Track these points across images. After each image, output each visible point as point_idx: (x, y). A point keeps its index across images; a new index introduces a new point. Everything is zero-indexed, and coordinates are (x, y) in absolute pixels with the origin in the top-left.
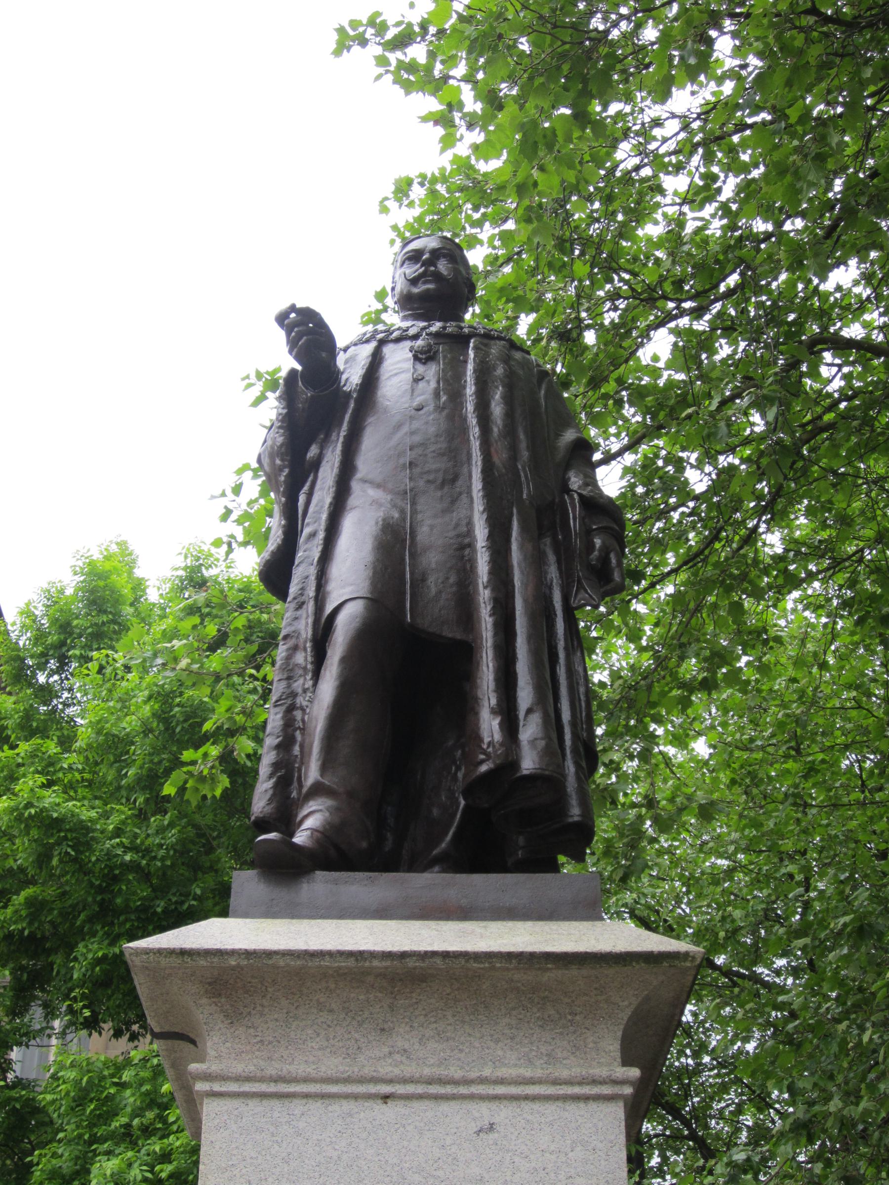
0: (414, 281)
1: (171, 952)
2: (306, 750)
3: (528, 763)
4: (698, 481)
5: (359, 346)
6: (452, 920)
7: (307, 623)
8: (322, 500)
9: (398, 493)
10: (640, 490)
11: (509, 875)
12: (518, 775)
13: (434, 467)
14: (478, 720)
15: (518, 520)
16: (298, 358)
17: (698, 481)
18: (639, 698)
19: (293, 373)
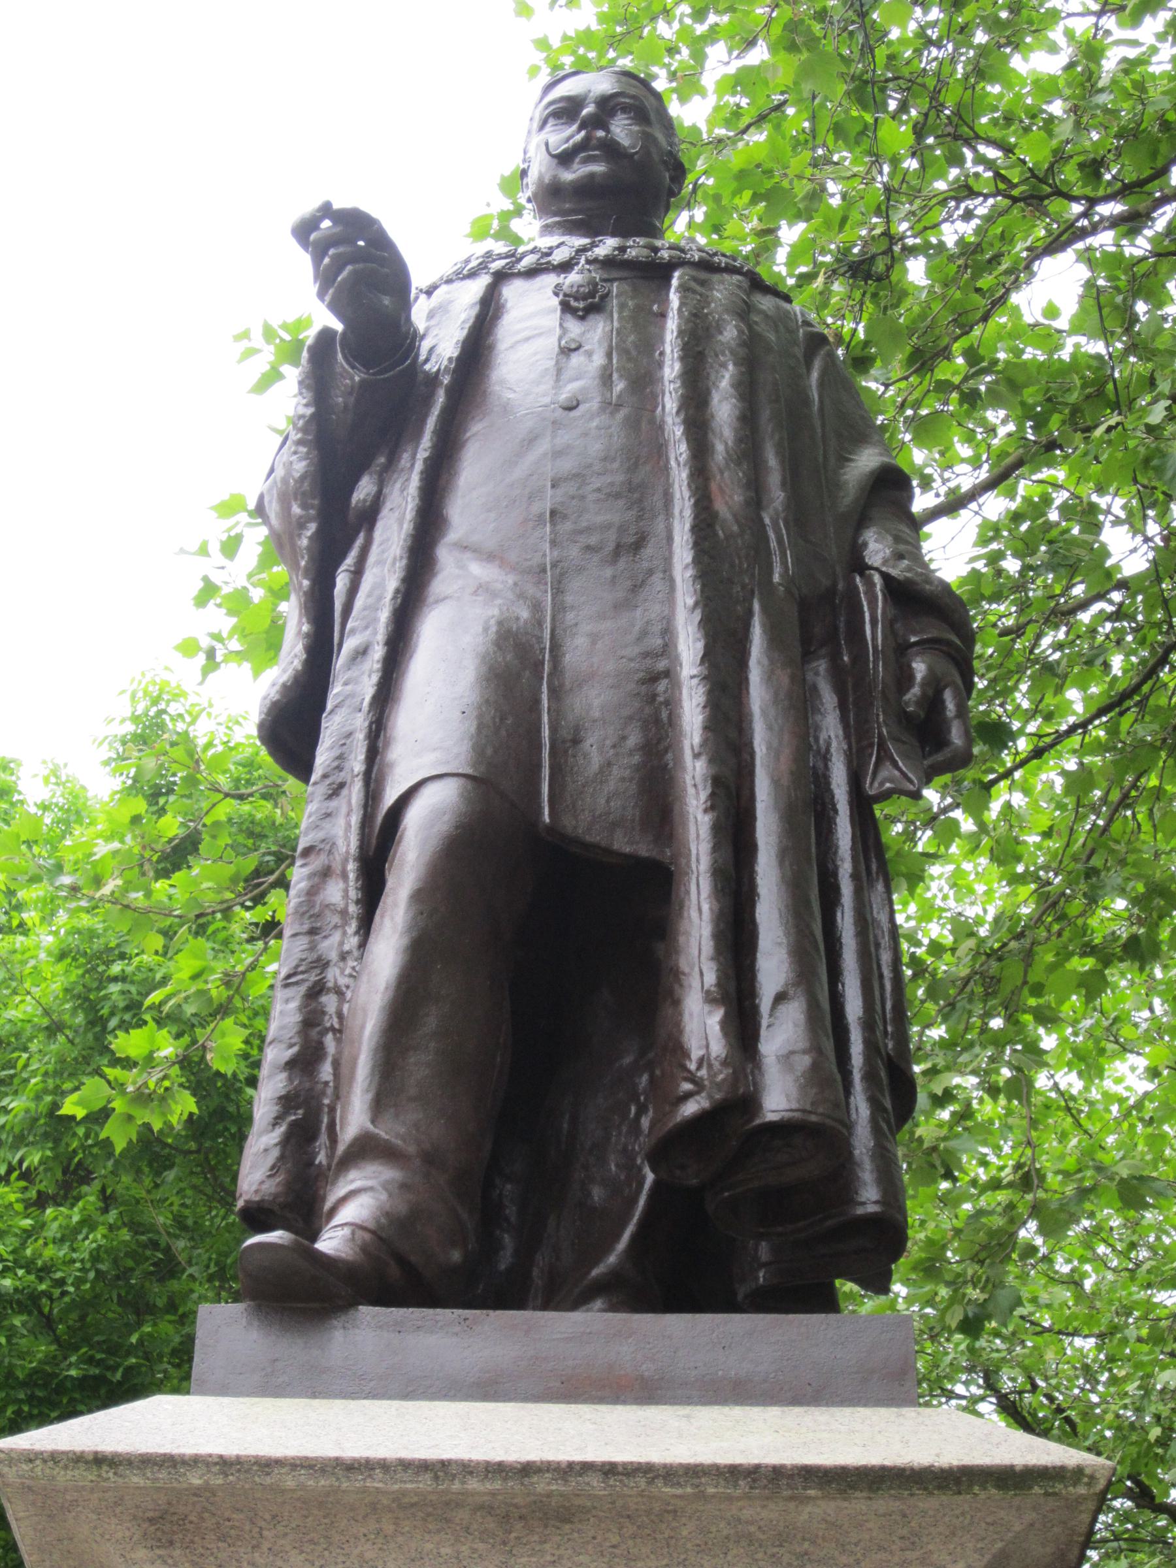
0: (564, 159)
1: (78, 1459)
2: (344, 1070)
3: (779, 1099)
4: (1127, 551)
5: (457, 285)
6: (624, 1403)
7: (349, 825)
8: (380, 585)
9: (528, 571)
10: (1012, 565)
11: (737, 1317)
12: (758, 1122)
13: (599, 519)
14: (681, 1014)
15: (763, 625)
16: (335, 307)
17: (1127, 551)
18: (1005, 976)
19: (326, 336)
